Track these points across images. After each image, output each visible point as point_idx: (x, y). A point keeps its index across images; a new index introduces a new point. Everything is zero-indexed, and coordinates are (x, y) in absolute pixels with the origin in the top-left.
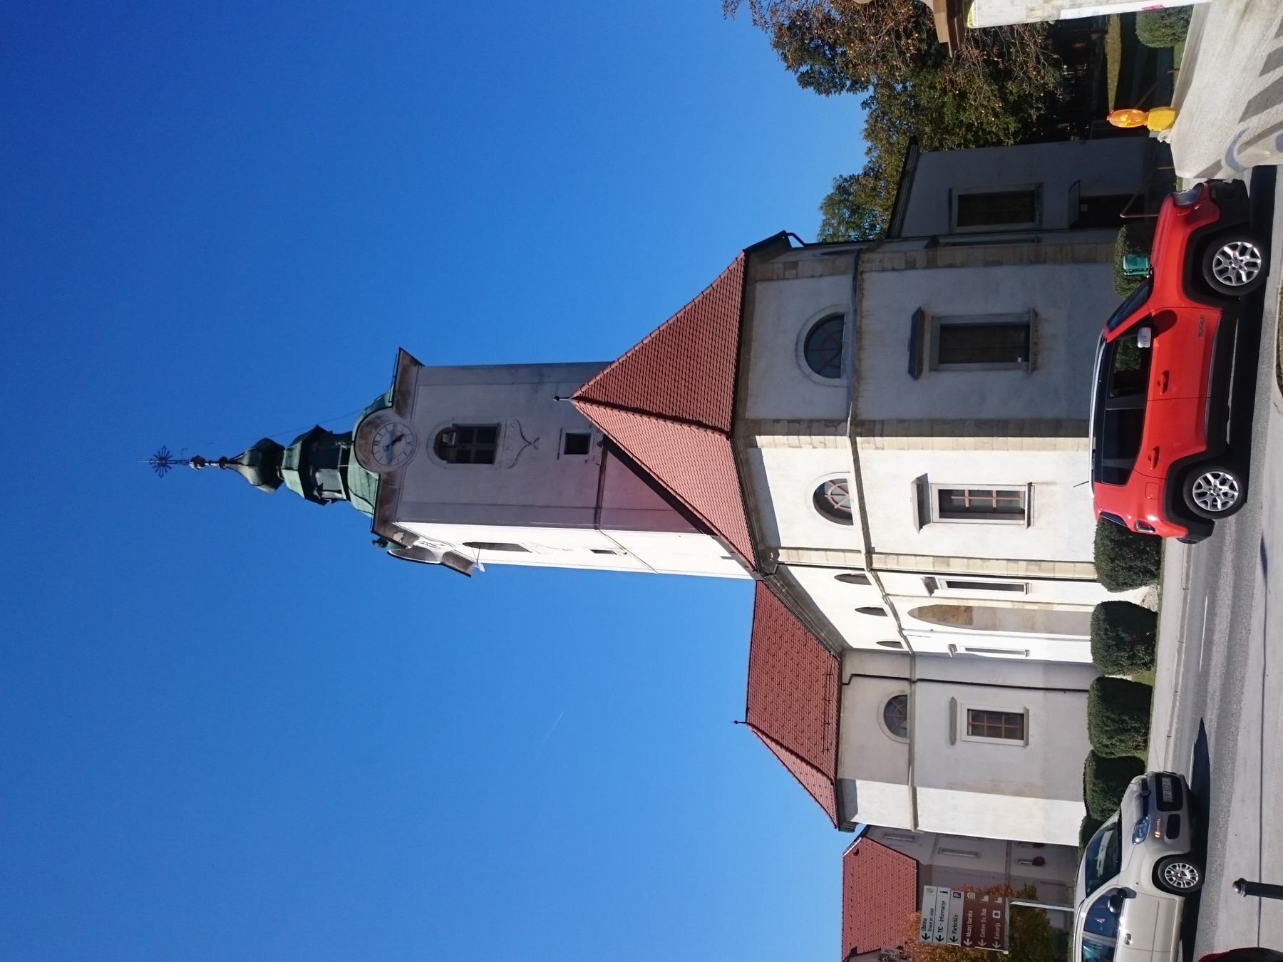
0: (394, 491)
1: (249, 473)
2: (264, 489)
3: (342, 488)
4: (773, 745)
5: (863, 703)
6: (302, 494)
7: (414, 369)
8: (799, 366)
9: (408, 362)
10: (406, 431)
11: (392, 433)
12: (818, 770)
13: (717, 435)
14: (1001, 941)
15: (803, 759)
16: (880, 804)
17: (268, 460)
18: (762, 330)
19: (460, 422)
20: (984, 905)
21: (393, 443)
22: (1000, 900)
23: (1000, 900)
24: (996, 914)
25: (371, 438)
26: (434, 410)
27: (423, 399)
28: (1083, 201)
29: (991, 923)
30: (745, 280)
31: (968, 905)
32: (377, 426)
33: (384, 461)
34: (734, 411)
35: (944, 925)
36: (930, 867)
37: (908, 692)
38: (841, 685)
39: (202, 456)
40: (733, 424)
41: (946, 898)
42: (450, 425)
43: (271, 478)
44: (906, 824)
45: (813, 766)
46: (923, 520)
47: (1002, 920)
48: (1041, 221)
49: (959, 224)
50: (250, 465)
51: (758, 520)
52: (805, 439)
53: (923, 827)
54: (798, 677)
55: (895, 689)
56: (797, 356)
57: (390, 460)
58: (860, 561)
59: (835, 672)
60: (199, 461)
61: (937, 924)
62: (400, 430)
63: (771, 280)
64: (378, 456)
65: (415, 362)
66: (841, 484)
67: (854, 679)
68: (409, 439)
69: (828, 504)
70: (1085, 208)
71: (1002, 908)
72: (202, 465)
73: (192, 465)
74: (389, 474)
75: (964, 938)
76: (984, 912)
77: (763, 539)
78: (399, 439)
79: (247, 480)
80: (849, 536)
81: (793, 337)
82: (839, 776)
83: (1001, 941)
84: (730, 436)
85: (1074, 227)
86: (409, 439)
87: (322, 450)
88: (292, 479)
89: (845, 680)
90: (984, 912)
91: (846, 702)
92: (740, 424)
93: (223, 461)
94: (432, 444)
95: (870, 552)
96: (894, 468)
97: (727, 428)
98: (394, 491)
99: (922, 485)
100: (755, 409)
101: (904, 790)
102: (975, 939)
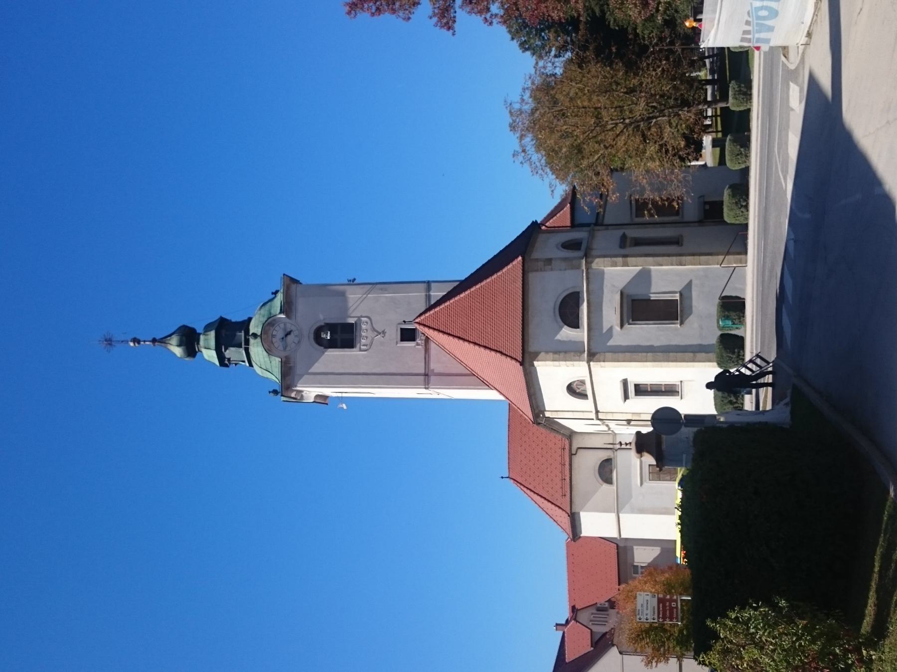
0: (290, 368)
1: (178, 351)
2: (187, 359)
3: (246, 359)
4: (528, 492)
5: (586, 465)
6: (217, 363)
7: (294, 286)
8: (557, 321)
9: (288, 281)
10: (293, 328)
11: (285, 329)
12: (560, 508)
13: (514, 362)
14: (677, 618)
15: (549, 501)
16: (596, 524)
17: (190, 339)
18: (535, 300)
19: (328, 321)
20: (668, 600)
21: (286, 335)
22: (675, 597)
23: (675, 597)
24: (673, 605)
25: (270, 332)
26: (310, 314)
27: (302, 306)
28: (706, 203)
29: (671, 609)
30: (523, 270)
31: (660, 601)
32: (273, 325)
33: (281, 348)
34: (523, 350)
35: (648, 612)
36: (625, 547)
37: (612, 456)
38: (571, 455)
39: (138, 337)
40: (523, 357)
41: (648, 598)
42: (323, 324)
43: (191, 349)
44: (615, 535)
45: (556, 505)
46: (626, 397)
47: (677, 608)
48: (683, 217)
49: (637, 216)
50: (179, 345)
51: (535, 399)
52: (562, 363)
53: (623, 536)
54: (543, 454)
55: (604, 455)
56: (555, 316)
57: (285, 348)
58: (593, 416)
59: (567, 447)
60: (136, 340)
61: (645, 612)
62: (289, 327)
63: (537, 271)
64: (276, 345)
65: (295, 281)
66: (583, 382)
67: (580, 451)
68: (296, 333)
69: (575, 390)
70: (707, 207)
71: (676, 601)
72: (139, 343)
73: (132, 344)
74: (286, 357)
75: (659, 618)
76: (668, 604)
77: (538, 407)
78: (289, 333)
79: (175, 355)
80: (588, 404)
81: (552, 304)
82: (573, 511)
83: (677, 618)
84: (522, 364)
85: (700, 222)
86: (296, 333)
87: (229, 333)
88: (210, 355)
89: (574, 452)
90: (668, 604)
91: (575, 465)
92: (526, 355)
93: (154, 341)
94: (312, 336)
95: (597, 412)
96: (609, 376)
97: (520, 359)
98: (290, 368)
99: (625, 383)
100: (532, 347)
101: (613, 516)
102: (664, 618)
